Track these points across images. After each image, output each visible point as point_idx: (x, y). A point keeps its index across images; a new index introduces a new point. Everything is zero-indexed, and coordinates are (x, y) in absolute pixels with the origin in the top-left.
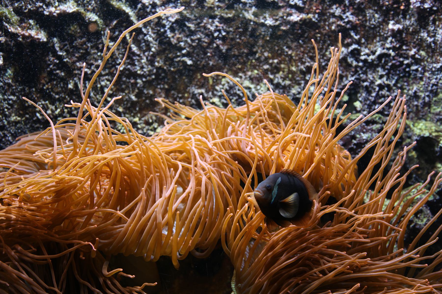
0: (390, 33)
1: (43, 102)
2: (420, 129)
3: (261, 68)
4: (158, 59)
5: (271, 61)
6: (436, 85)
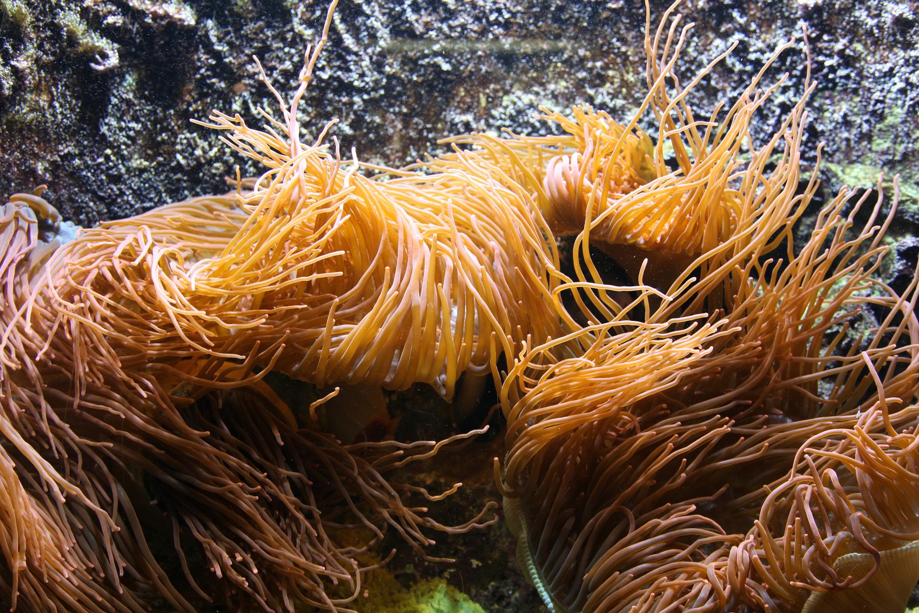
0: (799, 13)
1: (188, 135)
2: (856, 177)
3: (573, 77)
4: (391, 61)
5: (590, 65)
6: (882, 102)
